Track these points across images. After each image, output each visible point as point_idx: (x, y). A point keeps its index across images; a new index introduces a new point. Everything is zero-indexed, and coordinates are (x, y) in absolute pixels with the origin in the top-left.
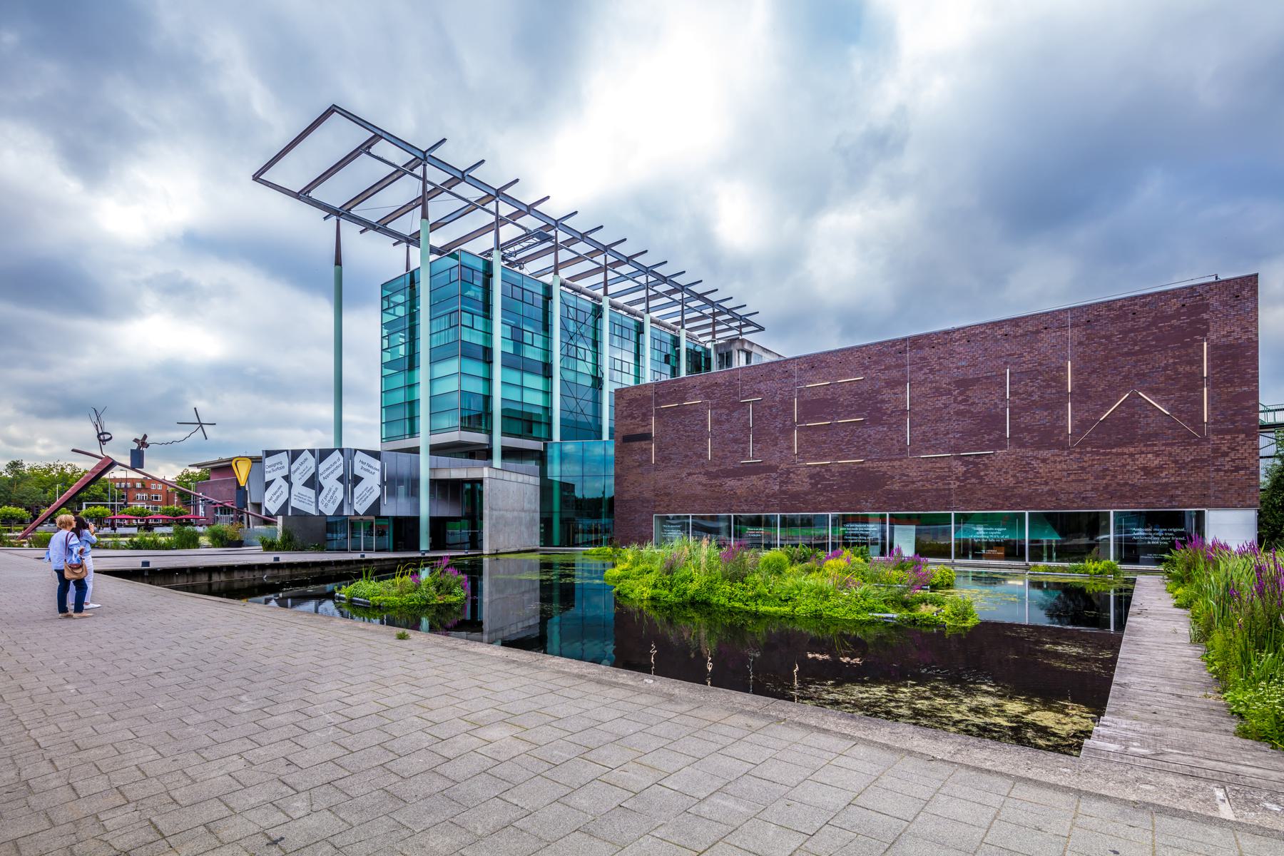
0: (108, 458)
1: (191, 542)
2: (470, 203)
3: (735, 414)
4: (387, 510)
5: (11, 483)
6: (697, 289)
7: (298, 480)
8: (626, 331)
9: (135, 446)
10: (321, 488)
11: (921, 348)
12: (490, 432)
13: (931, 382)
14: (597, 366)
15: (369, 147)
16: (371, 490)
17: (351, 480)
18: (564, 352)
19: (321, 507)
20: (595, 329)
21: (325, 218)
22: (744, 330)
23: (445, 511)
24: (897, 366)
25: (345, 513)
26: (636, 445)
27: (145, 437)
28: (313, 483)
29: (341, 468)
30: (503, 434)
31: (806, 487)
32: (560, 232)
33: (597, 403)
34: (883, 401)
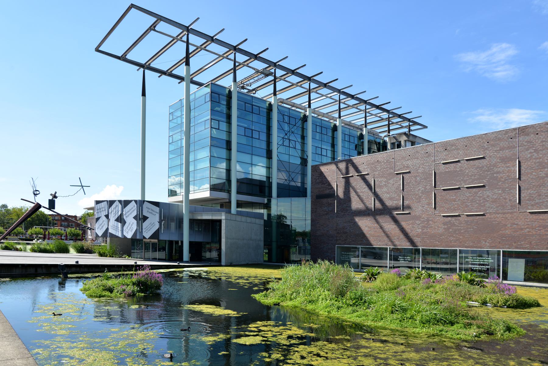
0: (38, 204)
1: (64, 250)
2: (220, 56)
3: (391, 181)
4: (164, 237)
5: (4, 215)
6: (376, 102)
7: (113, 218)
8: (324, 129)
9: (51, 198)
10: (125, 223)
11: (528, 135)
12: (229, 192)
13: (536, 159)
14: (303, 151)
15: (155, 27)
16: (153, 224)
17: (141, 219)
18: (281, 143)
19: (125, 234)
20: (303, 129)
21: (138, 70)
22: (412, 128)
23: (199, 239)
24: (509, 148)
25: (138, 238)
26: (325, 201)
27: (56, 193)
28: (120, 219)
29: (136, 211)
30: (238, 192)
31: (441, 231)
32: (277, 70)
33: (304, 175)
34: (498, 173)
